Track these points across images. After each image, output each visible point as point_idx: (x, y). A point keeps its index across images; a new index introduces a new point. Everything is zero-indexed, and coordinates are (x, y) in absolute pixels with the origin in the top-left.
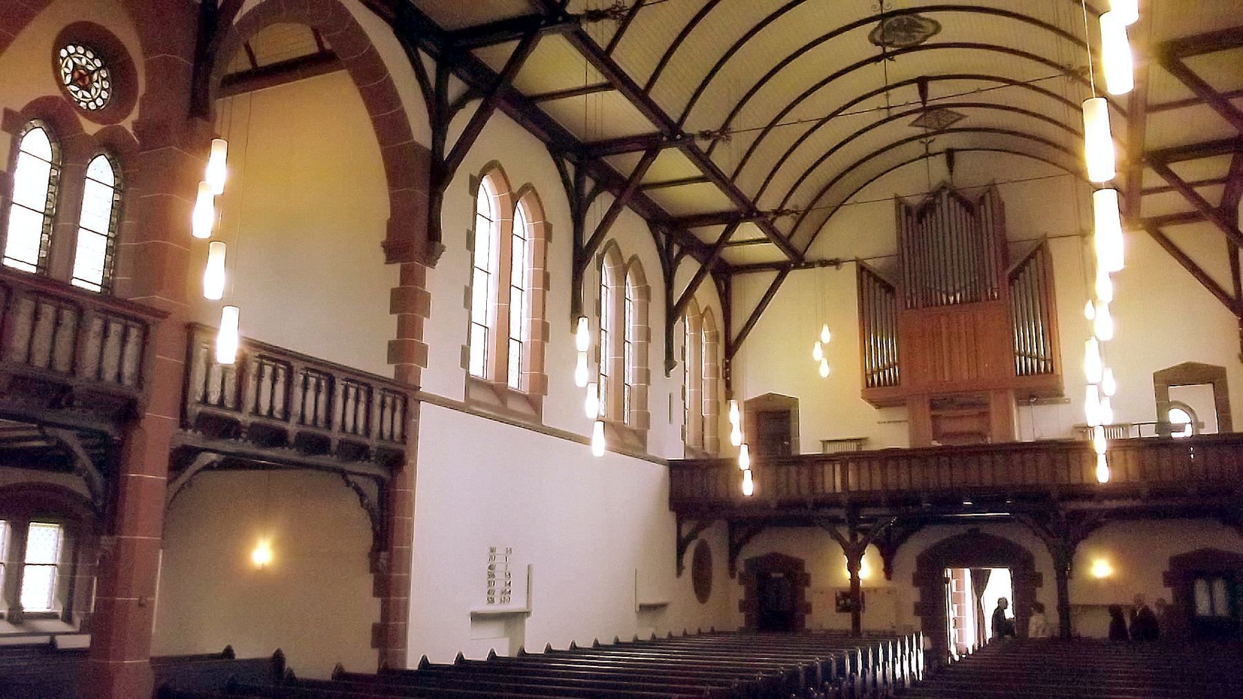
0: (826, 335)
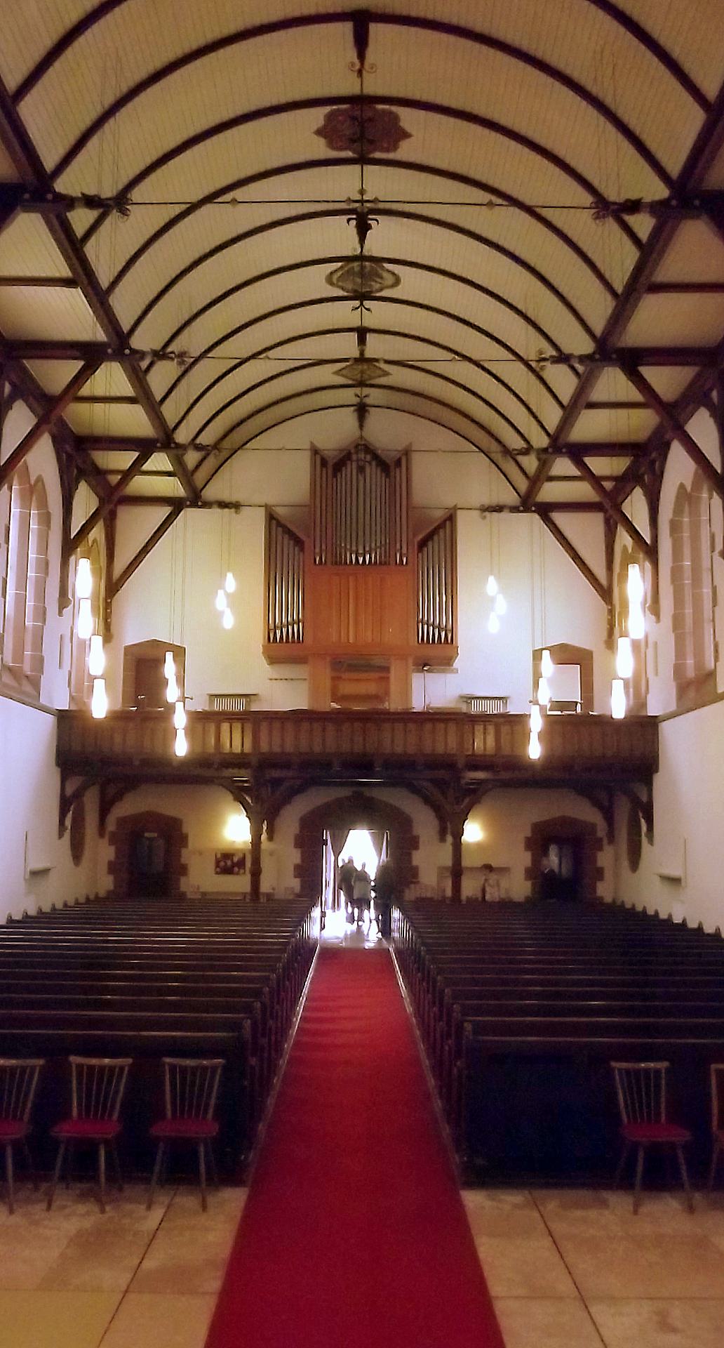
0: (231, 583)
